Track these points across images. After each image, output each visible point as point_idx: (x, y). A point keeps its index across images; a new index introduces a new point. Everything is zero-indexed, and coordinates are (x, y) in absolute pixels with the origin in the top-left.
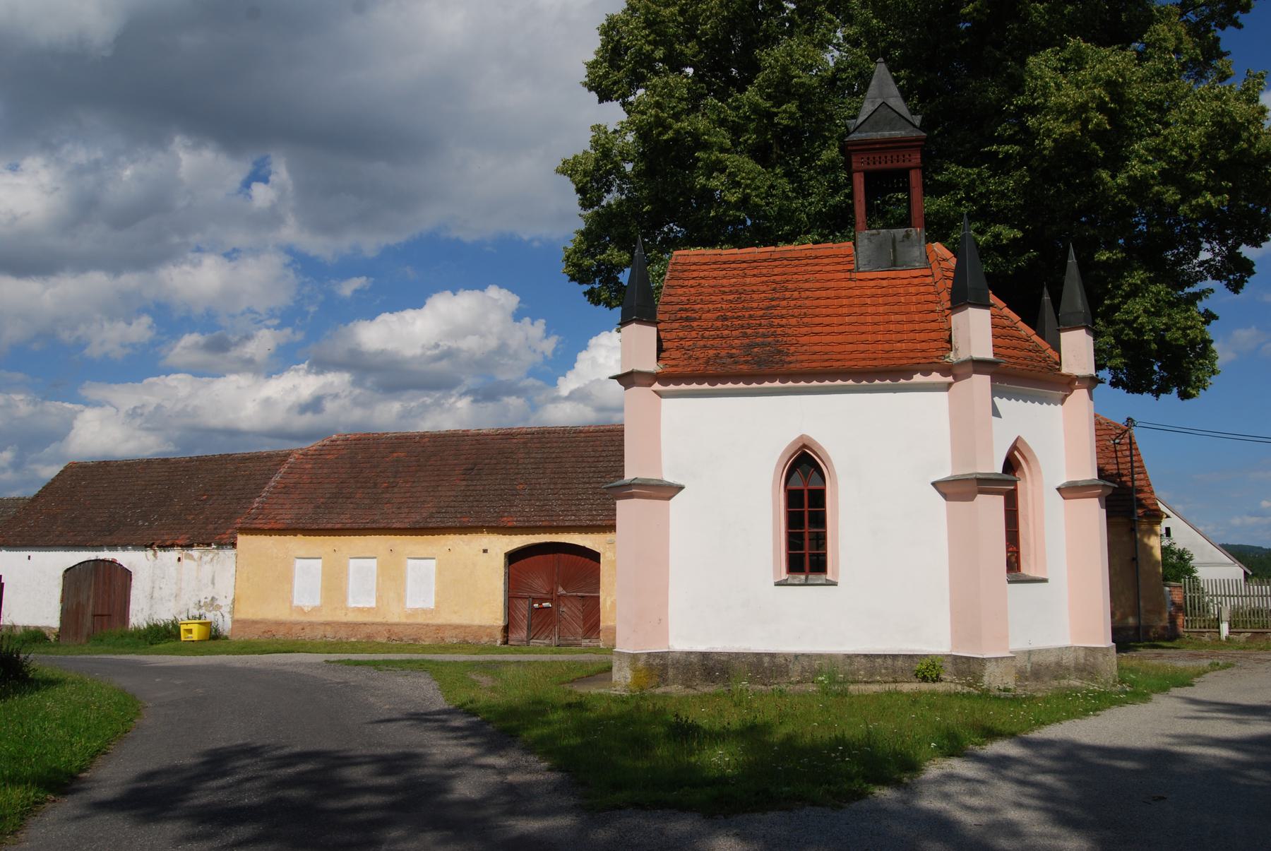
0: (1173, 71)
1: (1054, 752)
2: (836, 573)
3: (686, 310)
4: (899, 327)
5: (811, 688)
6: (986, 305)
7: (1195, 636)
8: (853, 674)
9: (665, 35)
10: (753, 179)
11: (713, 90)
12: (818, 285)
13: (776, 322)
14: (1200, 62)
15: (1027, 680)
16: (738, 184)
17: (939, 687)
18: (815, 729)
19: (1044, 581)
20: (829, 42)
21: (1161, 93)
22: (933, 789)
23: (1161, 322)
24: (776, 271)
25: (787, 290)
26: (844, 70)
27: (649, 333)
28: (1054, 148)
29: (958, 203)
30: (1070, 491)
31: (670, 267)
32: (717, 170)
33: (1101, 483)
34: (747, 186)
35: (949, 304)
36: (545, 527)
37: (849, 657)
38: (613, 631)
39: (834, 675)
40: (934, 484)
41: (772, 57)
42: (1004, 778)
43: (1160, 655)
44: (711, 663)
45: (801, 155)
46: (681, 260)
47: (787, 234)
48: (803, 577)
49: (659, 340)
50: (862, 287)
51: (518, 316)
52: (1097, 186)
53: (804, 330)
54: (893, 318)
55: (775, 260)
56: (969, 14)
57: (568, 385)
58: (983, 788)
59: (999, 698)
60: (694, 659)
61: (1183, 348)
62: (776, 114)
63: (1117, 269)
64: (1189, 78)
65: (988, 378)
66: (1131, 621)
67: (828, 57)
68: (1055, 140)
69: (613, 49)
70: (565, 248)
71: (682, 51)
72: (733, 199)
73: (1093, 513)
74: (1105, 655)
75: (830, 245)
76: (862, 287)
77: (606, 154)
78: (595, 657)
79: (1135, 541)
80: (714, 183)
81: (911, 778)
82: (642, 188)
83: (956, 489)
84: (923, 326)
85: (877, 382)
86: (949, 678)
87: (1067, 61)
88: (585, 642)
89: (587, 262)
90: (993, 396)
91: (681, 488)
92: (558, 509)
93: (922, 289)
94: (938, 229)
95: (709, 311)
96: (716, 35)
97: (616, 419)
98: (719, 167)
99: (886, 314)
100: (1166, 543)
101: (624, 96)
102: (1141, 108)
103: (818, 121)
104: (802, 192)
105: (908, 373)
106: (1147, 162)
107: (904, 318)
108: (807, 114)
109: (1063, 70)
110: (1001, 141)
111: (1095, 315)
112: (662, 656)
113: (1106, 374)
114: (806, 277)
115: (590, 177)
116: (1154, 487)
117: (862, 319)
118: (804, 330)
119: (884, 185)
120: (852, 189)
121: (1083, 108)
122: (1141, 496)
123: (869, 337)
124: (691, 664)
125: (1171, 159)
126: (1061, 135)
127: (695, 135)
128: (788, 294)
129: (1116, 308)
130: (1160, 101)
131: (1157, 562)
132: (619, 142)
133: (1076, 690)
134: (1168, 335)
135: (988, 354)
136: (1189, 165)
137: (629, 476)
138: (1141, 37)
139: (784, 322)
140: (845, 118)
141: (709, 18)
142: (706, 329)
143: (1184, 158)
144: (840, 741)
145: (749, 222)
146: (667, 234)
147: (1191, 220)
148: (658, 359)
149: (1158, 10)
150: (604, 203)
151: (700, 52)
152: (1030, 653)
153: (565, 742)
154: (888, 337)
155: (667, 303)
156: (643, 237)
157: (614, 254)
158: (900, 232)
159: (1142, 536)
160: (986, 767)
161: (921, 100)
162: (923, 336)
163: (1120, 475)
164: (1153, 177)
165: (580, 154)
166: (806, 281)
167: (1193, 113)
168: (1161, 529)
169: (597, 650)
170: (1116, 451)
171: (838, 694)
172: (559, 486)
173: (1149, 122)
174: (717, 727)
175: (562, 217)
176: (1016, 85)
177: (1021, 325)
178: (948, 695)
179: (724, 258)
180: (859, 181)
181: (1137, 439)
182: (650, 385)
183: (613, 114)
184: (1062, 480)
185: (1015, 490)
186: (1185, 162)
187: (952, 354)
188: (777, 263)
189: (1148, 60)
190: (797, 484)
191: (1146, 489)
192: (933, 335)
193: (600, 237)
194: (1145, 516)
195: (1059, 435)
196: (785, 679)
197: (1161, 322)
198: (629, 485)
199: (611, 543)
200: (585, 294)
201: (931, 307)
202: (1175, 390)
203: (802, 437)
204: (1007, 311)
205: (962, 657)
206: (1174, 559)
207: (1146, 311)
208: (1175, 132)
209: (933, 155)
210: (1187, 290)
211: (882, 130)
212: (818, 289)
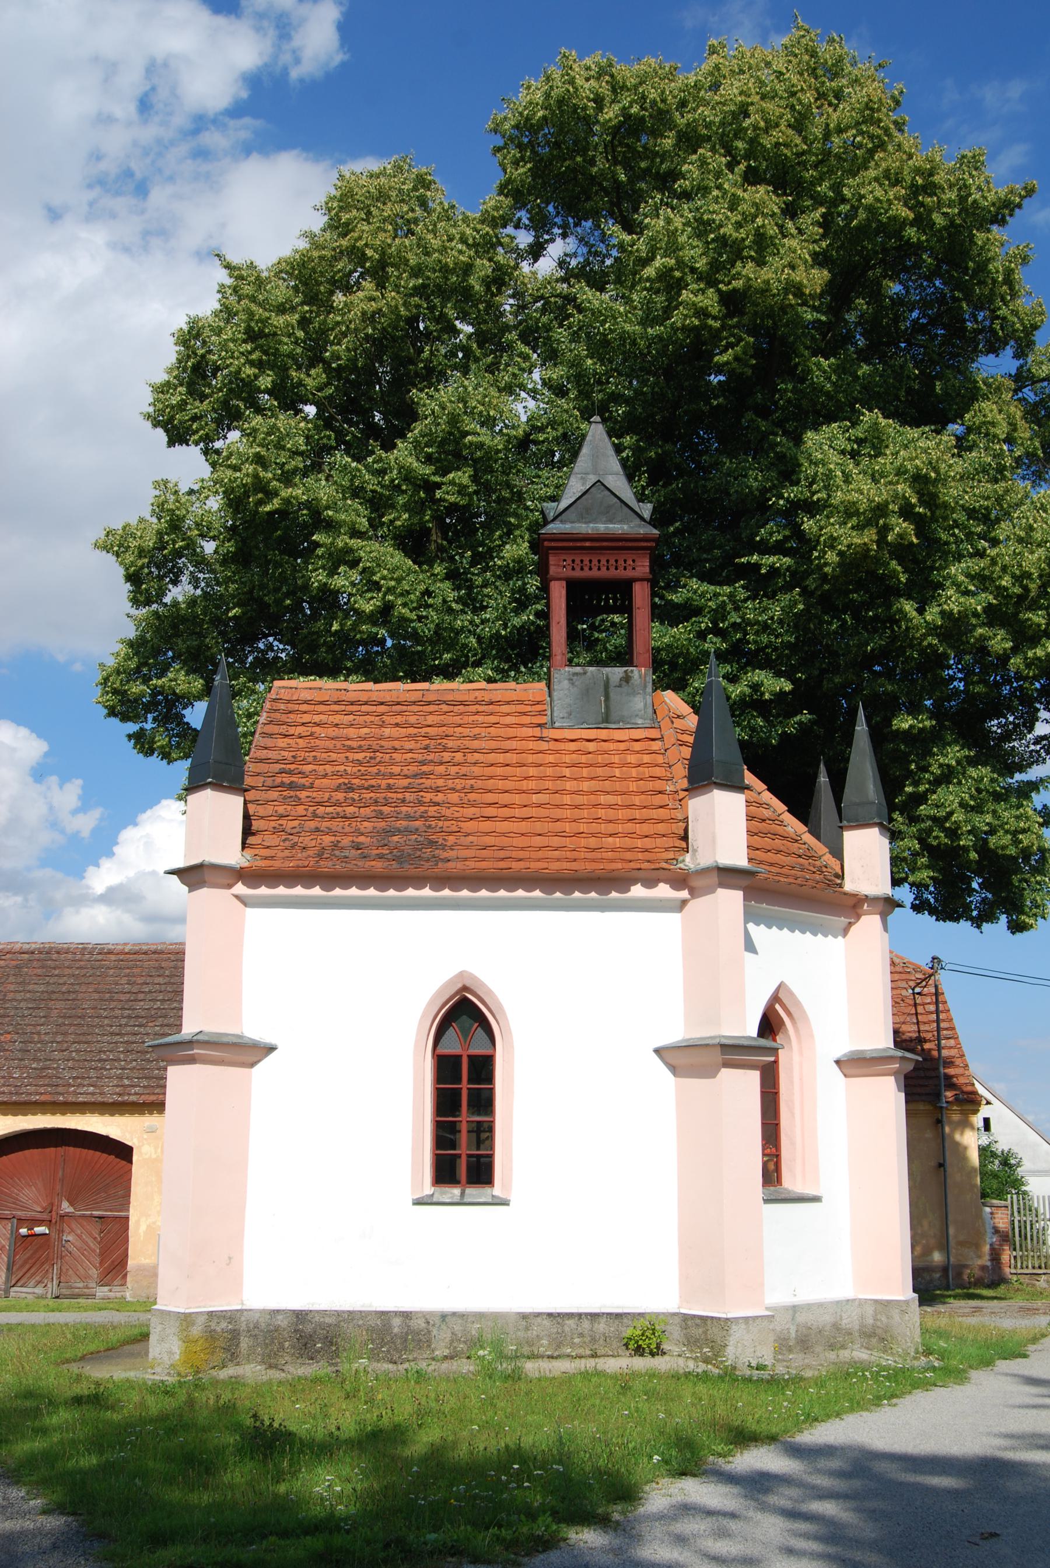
0: (1004, 468)
1: (835, 1464)
2: (507, 1186)
3: (290, 772)
4: (611, 814)
5: (466, 1367)
6: (740, 787)
7: (1025, 1280)
8: (530, 1343)
9: (277, 353)
10: (399, 580)
11: (345, 443)
12: (493, 744)
13: (428, 796)
14: (1039, 459)
15: (790, 1350)
16: (376, 586)
17: (660, 1363)
18: (477, 1439)
19: (816, 1199)
20: (522, 387)
21: (988, 498)
22: (658, 1529)
23: (983, 821)
24: (430, 719)
25: (445, 749)
26: (541, 429)
27: (232, 805)
28: (840, 565)
29: (702, 635)
30: (855, 1064)
31: (267, 705)
32: (346, 563)
33: (899, 1053)
34: (390, 590)
35: (685, 783)
36: (43, 1104)
37: (524, 1316)
38: (152, 1274)
39: (498, 1346)
40: (657, 1051)
41: (435, 402)
42: (764, 1507)
43: (977, 1310)
44: (309, 1328)
45: (473, 548)
46: (284, 695)
47: (447, 665)
48: (456, 1191)
49: (247, 817)
50: (557, 752)
51: (39, 773)
52: (897, 622)
53: (470, 812)
54: (603, 799)
55: (429, 703)
56: (727, 363)
57: (103, 877)
58: (733, 1525)
59: (749, 1380)
60: (282, 1322)
61: (1014, 859)
62: (438, 486)
63: (922, 743)
64: (1023, 478)
65: (739, 894)
66: (937, 1257)
67: (519, 407)
68: (841, 554)
69: (196, 368)
70: (102, 665)
71: (301, 381)
72: (368, 608)
73: (886, 1098)
74: (904, 1312)
75: (512, 685)
76: (557, 752)
77: (175, 525)
78: (119, 1317)
79: (942, 1137)
80: (338, 582)
81: (623, 1513)
82: (228, 580)
83: (692, 1059)
84: (646, 813)
85: (577, 894)
86: (676, 1350)
87: (860, 442)
88: (102, 1291)
89: (136, 688)
90: (746, 922)
91: (271, 1049)
92: (67, 1074)
93: (646, 758)
94: (673, 671)
95: (325, 776)
96: (354, 360)
97: (171, 934)
98: (346, 558)
99: (592, 793)
100: (984, 1140)
101: (208, 439)
102: (960, 516)
103: (500, 500)
104: (473, 603)
105: (622, 882)
106: (967, 593)
107: (619, 800)
108: (486, 489)
109: (854, 455)
110: (765, 549)
111: (892, 807)
112: (231, 1316)
113: (905, 894)
114: (477, 731)
115: (150, 561)
116: (968, 1058)
117: (557, 799)
118: (470, 812)
119: (591, 600)
120: (548, 605)
121: (881, 510)
122: (951, 1071)
123: (568, 827)
124: (277, 1329)
125: (1000, 591)
126: (849, 546)
127: (314, 509)
128: (447, 756)
129: (920, 799)
130: (987, 508)
131: (974, 1169)
132: (196, 509)
133: (864, 1366)
134: (992, 841)
135: (741, 860)
136: (1022, 600)
137: (190, 1027)
138: (962, 417)
139: (440, 798)
140: (542, 499)
141: (344, 335)
142: (319, 804)
143: (1017, 590)
144: (515, 1454)
145: (389, 643)
146: (264, 652)
147: (1026, 678)
148: (244, 845)
149: (985, 383)
150: (167, 600)
151: (328, 384)
152: (795, 1309)
153: (71, 1464)
154: (594, 827)
155: (261, 761)
156: (227, 656)
157: (180, 679)
158: (616, 673)
159: (953, 1131)
160: (736, 1490)
161: (652, 482)
162: (645, 829)
163: (921, 1040)
164: (976, 615)
165: (134, 522)
166: (475, 737)
167: (1031, 528)
168: (978, 1120)
169: (122, 1305)
170: (915, 1005)
171: (507, 1377)
172: (71, 1038)
173: (969, 535)
174: (320, 1434)
175: (105, 620)
176: (789, 472)
177: (788, 818)
178: (676, 1377)
179: (351, 696)
180: (558, 593)
181: (944, 987)
182: (230, 886)
183: (189, 466)
184: (843, 1049)
185: (776, 1062)
186: (1019, 596)
187: (688, 857)
188: (432, 708)
189: (970, 449)
190: (452, 1045)
191: (958, 1062)
192: (661, 828)
193: (157, 652)
194: (957, 1100)
195: (839, 982)
196: (427, 1354)
197: (983, 821)
198: (190, 1043)
199: (152, 1131)
200: (130, 737)
201: (658, 785)
202: (1003, 918)
203: (461, 974)
204: (768, 797)
205: (694, 1317)
206: (996, 1165)
207: (963, 805)
208: (1005, 552)
209: (667, 562)
210: (1018, 776)
211: (594, 521)
212: (493, 751)
